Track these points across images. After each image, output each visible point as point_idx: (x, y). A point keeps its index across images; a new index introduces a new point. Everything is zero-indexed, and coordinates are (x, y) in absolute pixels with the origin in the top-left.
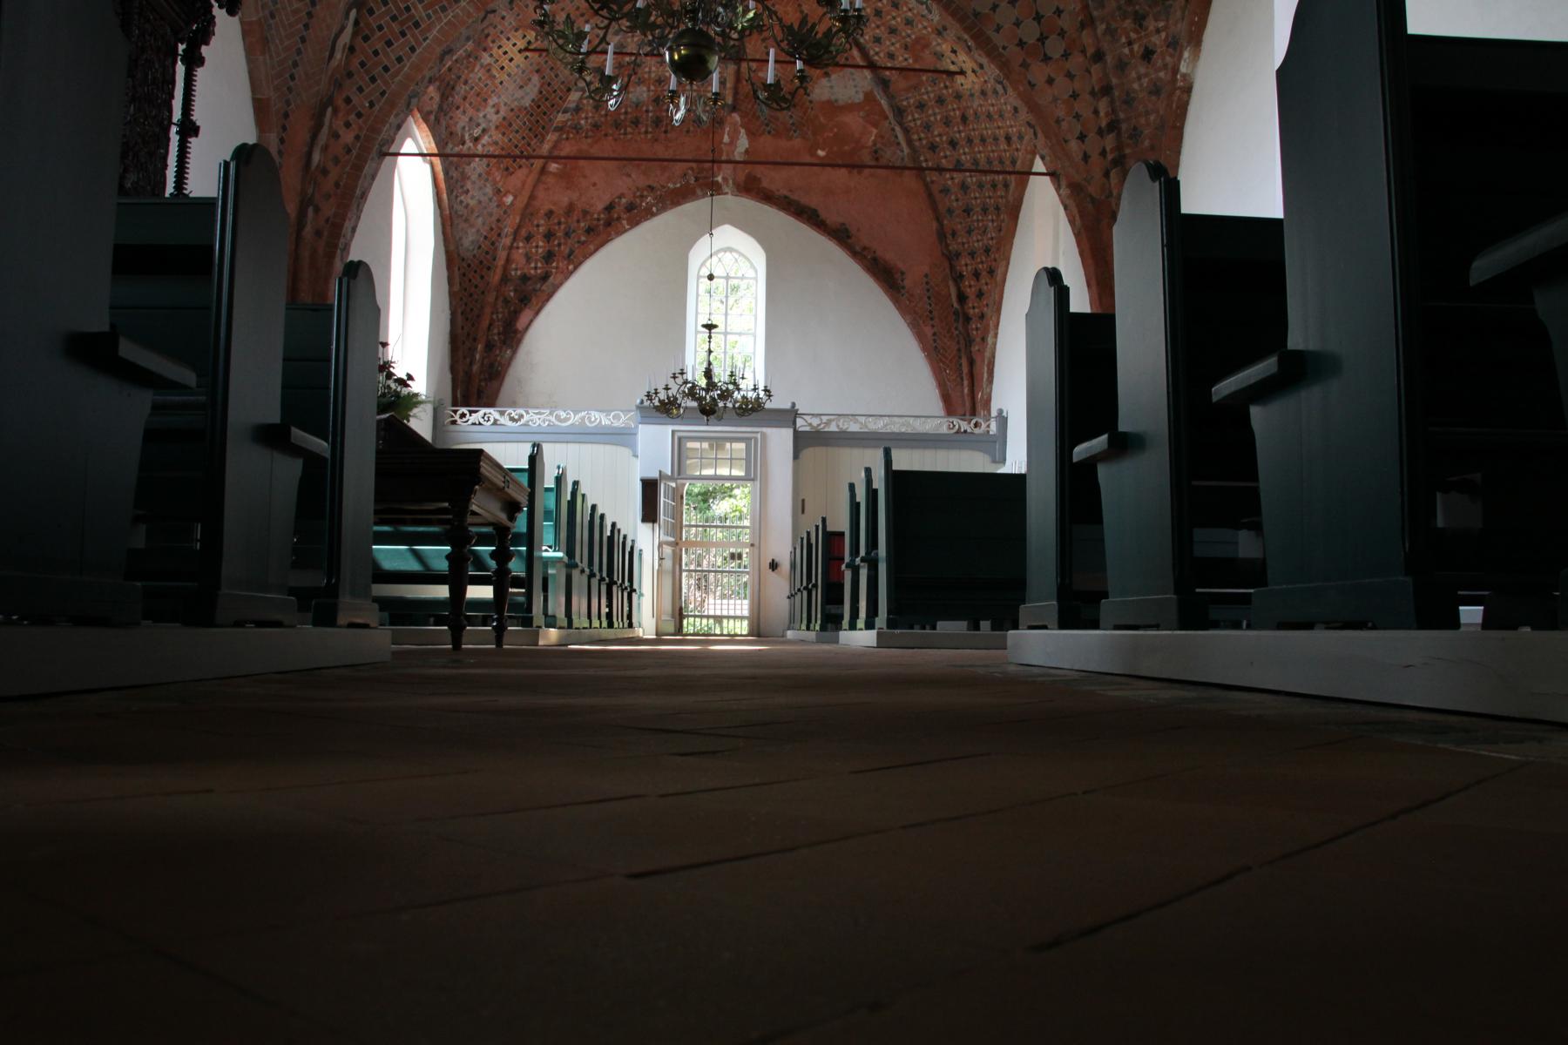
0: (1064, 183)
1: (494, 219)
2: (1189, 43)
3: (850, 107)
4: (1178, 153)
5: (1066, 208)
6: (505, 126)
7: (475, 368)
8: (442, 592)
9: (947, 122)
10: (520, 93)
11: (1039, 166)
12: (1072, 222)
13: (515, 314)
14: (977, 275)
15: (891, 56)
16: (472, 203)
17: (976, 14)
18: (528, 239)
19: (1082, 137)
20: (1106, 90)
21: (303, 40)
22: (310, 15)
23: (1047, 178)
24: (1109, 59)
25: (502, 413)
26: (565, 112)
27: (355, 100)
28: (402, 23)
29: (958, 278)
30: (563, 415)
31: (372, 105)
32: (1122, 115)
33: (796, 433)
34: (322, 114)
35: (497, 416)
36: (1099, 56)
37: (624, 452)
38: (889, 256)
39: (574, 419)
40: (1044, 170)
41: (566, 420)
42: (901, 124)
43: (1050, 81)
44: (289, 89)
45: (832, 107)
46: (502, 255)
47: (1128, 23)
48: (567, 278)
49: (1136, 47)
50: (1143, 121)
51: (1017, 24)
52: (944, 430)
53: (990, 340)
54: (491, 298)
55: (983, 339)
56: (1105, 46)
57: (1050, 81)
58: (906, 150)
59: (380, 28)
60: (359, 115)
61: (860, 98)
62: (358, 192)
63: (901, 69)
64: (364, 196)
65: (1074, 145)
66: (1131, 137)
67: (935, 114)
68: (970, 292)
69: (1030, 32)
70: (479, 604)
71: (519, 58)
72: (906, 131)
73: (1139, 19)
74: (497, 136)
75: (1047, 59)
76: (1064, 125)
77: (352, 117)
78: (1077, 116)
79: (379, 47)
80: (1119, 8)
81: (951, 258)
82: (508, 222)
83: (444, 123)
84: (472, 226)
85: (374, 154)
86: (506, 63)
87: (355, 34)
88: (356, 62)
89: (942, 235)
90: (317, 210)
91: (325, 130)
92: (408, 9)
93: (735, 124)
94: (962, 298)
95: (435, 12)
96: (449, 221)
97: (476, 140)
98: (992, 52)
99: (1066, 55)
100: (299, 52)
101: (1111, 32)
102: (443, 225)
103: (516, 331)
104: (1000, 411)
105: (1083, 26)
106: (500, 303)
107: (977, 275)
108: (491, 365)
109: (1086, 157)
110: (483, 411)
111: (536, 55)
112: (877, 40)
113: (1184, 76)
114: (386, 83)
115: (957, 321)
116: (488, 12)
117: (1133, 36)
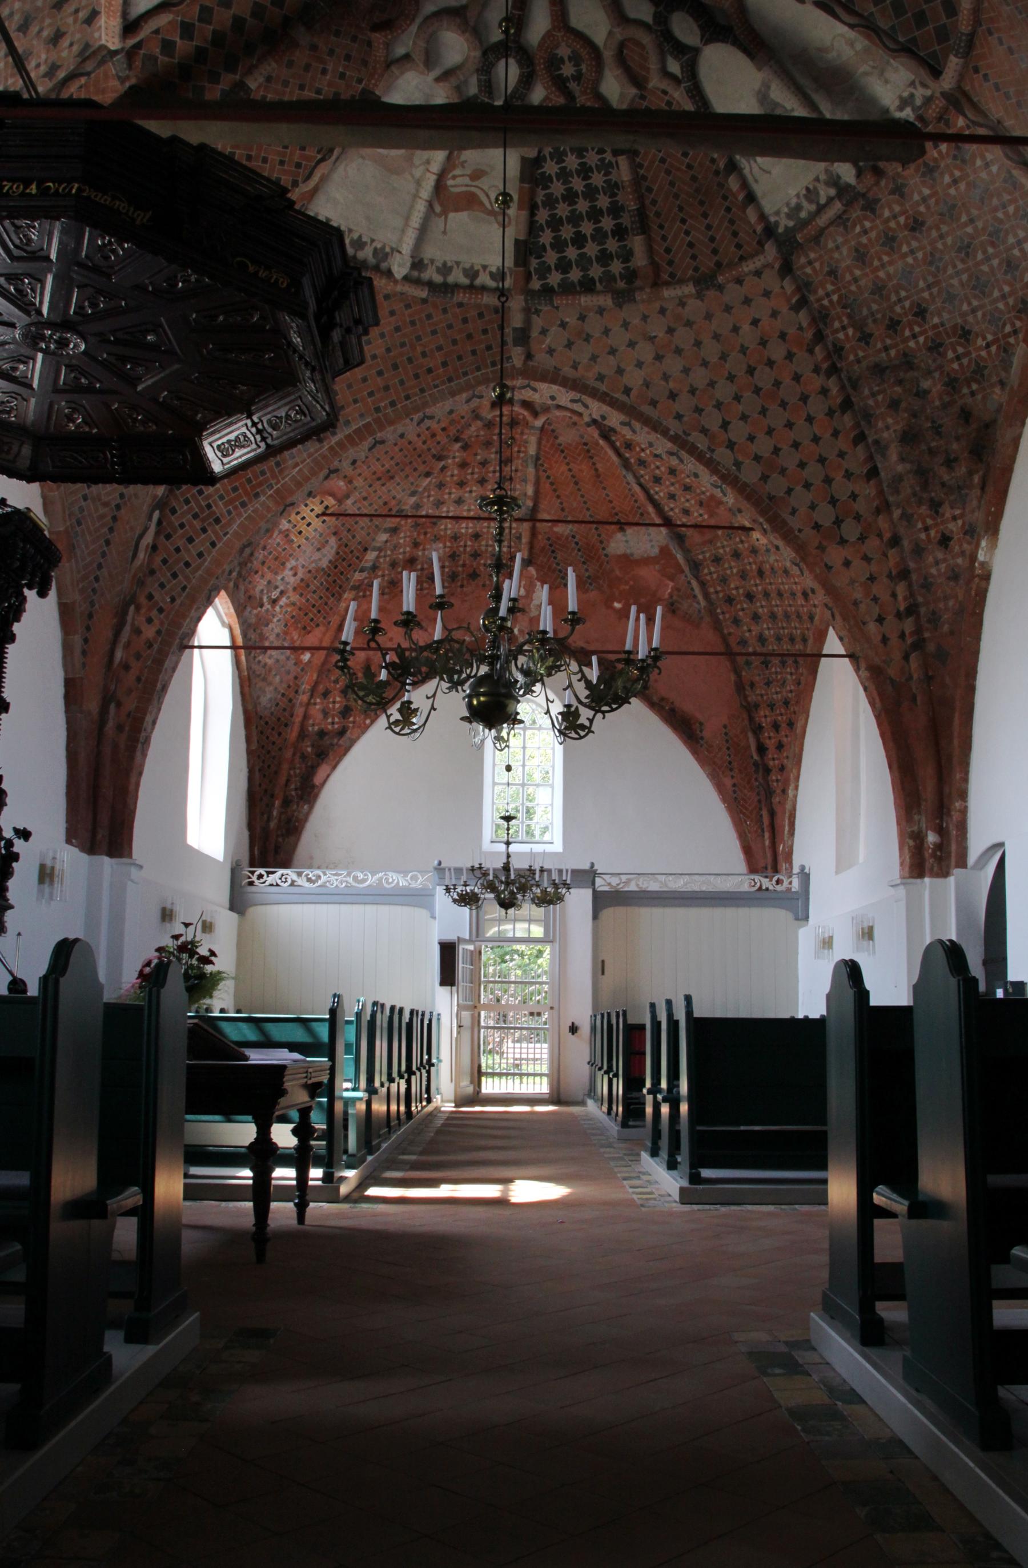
0: (863, 666)
1: (291, 676)
2: (986, 532)
3: (646, 561)
4: (978, 638)
5: (865, 689)
6: (303, 587)
7: (273, 825)
8: (245, 1174)
9: (743, 575)
10: (317, 555)
11: (833, 643)
12: (872, 704)
13: (312, 770)
14: (776, 727)
15: (686, 512)
16: (270, 662)
17: (771, 498)
18: (326, 694)
19: (880, 620)
20: (904, 574)
21: (108, 543)
22: (115, 519)
23: (847, 660)
24: (905, 543)
25: (299, 874)
26: (362, 571)
27: (157, 596)
28: (203, 520)
29: (758, 730)
30: (361, 876)
31: (173, 600)
32: (920, 599)
33: (594, 891)
34: (124, 613)
35: (294, 877)
36: (895, 541)
37: (421, 913)
38: (687, 707)
39: (371, 880)
40: (844, 653)
41: (364, 881)
42: (697, 577)
43: (847, 564)
44: (94, 590)
45: (627, 561)
46: (299, 711)
47: (924, 510)
48: (363, 733)
49: (932, 533)
50: (941, 605)
51: (813, 507)
52: (745, 887)
53: (791, 792)
54: (288, 754)
55: (784, 791)
56: (902, 531)
57: (847, 564)
58: (703, 603)
59: (182, 526)
60: (161, 610)
61: (655, 552)
62: (159, 686)
63: (695, 526)
64: (165, 688)
65: (872, 627)
66: (929, 621)
67: (733, 568)
68: (771, 744)
69: (825, 515)
70: (619, 602)
71: (317, 523)
72: (703, 584)
73: (935, 506)
74: (295, 598)
75: (843, 542)
76: (863, 607)
77: (154, 613)
78: (875, 599)
79: (180, 543)
80: (915, 494)
81: (750, 709)
82: (306, 678)
83: (242, 588)
84: (270, 684)
85: (174, 647)
86: (303, 527)
87: (158, 533)
88: (158, 560)
89: (740, 687)
90: (119, 705)
91: (127, 628)
92: (209, 506)
93: (531, 578)
94: (762, 749)
95: (236, 508)
96: (247, 684)
97: (274, 602)
98: (788, 535)
99: (862, 538)
100: (104, 555)
101: (906, 517)
102: (242, 687)
103: (313, 786)
104: (803, 868)
105: (878, 511)
106: (297, 759)
107: (776, 727)
108: (289, 821)
109: (885, 640)
110: (281, 872)
111: (334, 519)
112: (672, 497)
113: (983, 564)
114: (187, 578)
115: (756, 771)
116: (287, 506)
117: (929, 522)
